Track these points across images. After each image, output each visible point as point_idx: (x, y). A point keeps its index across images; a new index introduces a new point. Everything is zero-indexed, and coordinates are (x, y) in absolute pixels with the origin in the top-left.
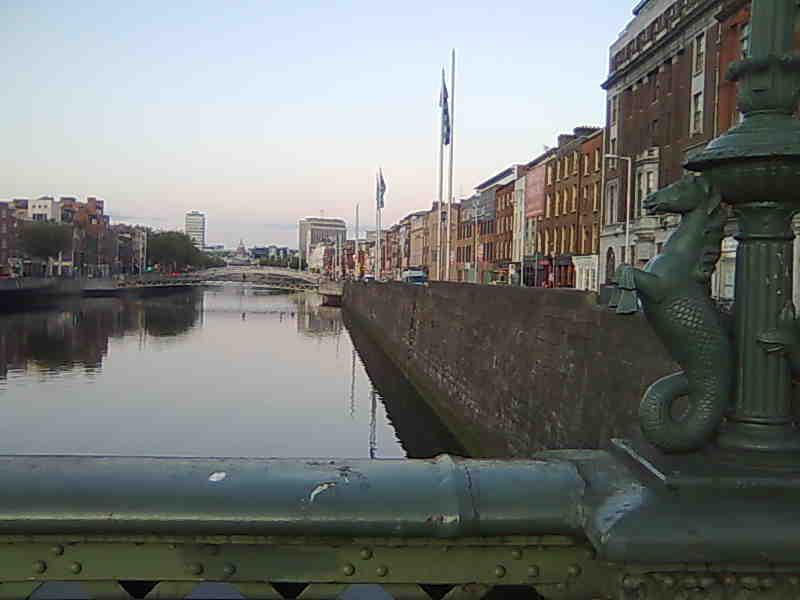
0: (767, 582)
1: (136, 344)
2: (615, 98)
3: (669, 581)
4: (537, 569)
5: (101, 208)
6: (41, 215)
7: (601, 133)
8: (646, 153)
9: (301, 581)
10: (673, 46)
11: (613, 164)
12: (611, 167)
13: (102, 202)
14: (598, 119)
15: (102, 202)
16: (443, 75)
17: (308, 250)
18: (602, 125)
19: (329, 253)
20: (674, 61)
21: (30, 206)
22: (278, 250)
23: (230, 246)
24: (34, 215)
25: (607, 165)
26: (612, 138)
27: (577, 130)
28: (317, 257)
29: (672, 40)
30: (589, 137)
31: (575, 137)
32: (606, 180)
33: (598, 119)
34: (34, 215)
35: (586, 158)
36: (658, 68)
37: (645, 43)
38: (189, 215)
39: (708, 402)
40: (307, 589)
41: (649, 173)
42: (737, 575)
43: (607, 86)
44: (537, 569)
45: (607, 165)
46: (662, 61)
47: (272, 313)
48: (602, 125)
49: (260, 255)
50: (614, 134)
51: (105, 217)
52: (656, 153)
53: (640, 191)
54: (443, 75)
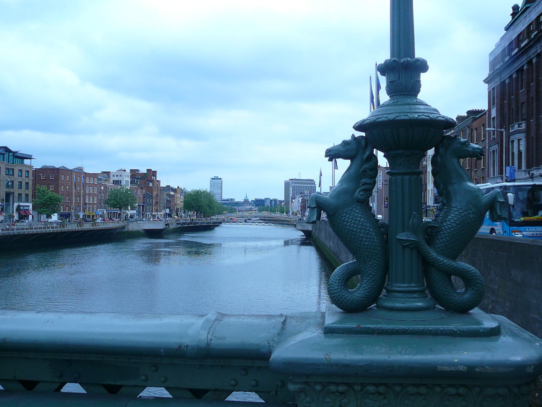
0: (381, 389)
1: (316, 267)
2: (493, 89)
3: (318, 387)
4: (257, 382)
5: (155, 176)
6: (118, 181)
7: (486, 113)
8: (516, 126)
9: (119, 383)
10: (533, 51)
11: (494, 135)
12: (492, 137)
13: (156, 172)
14: (483, 105)
15: (156, 172)
16: (371, 79)
17: (290, 200)
18: (486, 108)
19: (304, 201)
20: (534, 61)
21: (111, 176)
22: (271, 201)
23: (239, 199)
24: (114, 181)
25: (489, 136)
26: (492, 117)
27: (468, 112)
28: (296, 205)
29: (532, 47)
30: (477, 116)
31: (467, 117)
32: (489, 147)
33: (483, 105)
34: (114, 181)
35: (475, 131)
36: (523, 66)
37: (513, 50)
38: (212, 179)
39: (368, 278)
40: (208, 394)
41: (519, 140)
42: (363, 385)
43: (486, 81)
44: (257, 382)
45: (489, 136)
46: (526, 62)
47: (257, 238)
48: (486, 108)
49: (259, 203)
50: (494, 114)
51: (158, 181)
52: (524, 126)
53: (513, 153)
54: (371, 79)
